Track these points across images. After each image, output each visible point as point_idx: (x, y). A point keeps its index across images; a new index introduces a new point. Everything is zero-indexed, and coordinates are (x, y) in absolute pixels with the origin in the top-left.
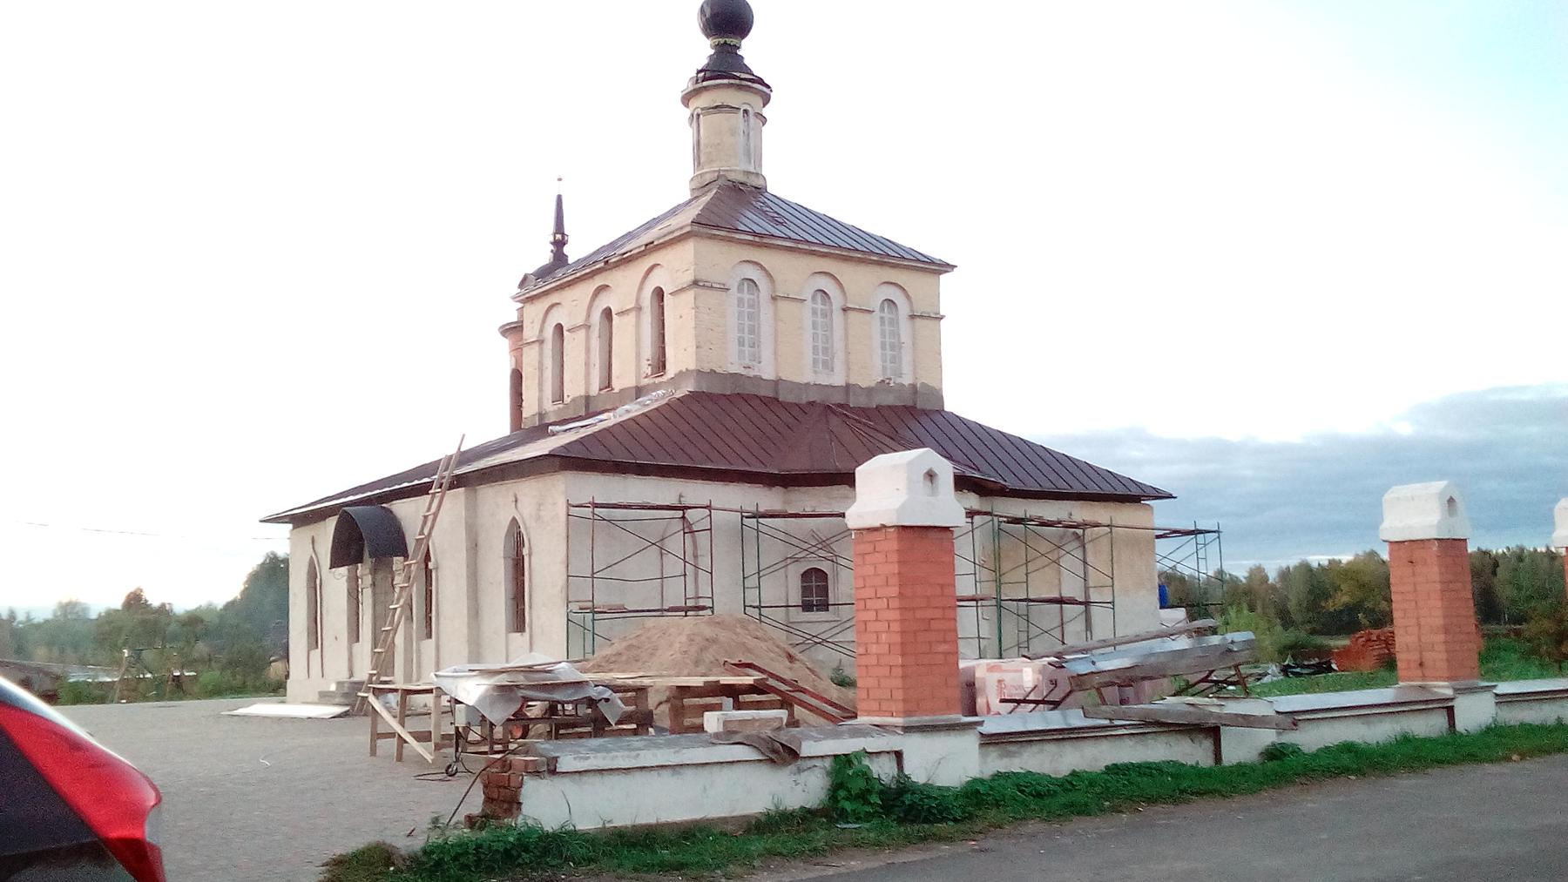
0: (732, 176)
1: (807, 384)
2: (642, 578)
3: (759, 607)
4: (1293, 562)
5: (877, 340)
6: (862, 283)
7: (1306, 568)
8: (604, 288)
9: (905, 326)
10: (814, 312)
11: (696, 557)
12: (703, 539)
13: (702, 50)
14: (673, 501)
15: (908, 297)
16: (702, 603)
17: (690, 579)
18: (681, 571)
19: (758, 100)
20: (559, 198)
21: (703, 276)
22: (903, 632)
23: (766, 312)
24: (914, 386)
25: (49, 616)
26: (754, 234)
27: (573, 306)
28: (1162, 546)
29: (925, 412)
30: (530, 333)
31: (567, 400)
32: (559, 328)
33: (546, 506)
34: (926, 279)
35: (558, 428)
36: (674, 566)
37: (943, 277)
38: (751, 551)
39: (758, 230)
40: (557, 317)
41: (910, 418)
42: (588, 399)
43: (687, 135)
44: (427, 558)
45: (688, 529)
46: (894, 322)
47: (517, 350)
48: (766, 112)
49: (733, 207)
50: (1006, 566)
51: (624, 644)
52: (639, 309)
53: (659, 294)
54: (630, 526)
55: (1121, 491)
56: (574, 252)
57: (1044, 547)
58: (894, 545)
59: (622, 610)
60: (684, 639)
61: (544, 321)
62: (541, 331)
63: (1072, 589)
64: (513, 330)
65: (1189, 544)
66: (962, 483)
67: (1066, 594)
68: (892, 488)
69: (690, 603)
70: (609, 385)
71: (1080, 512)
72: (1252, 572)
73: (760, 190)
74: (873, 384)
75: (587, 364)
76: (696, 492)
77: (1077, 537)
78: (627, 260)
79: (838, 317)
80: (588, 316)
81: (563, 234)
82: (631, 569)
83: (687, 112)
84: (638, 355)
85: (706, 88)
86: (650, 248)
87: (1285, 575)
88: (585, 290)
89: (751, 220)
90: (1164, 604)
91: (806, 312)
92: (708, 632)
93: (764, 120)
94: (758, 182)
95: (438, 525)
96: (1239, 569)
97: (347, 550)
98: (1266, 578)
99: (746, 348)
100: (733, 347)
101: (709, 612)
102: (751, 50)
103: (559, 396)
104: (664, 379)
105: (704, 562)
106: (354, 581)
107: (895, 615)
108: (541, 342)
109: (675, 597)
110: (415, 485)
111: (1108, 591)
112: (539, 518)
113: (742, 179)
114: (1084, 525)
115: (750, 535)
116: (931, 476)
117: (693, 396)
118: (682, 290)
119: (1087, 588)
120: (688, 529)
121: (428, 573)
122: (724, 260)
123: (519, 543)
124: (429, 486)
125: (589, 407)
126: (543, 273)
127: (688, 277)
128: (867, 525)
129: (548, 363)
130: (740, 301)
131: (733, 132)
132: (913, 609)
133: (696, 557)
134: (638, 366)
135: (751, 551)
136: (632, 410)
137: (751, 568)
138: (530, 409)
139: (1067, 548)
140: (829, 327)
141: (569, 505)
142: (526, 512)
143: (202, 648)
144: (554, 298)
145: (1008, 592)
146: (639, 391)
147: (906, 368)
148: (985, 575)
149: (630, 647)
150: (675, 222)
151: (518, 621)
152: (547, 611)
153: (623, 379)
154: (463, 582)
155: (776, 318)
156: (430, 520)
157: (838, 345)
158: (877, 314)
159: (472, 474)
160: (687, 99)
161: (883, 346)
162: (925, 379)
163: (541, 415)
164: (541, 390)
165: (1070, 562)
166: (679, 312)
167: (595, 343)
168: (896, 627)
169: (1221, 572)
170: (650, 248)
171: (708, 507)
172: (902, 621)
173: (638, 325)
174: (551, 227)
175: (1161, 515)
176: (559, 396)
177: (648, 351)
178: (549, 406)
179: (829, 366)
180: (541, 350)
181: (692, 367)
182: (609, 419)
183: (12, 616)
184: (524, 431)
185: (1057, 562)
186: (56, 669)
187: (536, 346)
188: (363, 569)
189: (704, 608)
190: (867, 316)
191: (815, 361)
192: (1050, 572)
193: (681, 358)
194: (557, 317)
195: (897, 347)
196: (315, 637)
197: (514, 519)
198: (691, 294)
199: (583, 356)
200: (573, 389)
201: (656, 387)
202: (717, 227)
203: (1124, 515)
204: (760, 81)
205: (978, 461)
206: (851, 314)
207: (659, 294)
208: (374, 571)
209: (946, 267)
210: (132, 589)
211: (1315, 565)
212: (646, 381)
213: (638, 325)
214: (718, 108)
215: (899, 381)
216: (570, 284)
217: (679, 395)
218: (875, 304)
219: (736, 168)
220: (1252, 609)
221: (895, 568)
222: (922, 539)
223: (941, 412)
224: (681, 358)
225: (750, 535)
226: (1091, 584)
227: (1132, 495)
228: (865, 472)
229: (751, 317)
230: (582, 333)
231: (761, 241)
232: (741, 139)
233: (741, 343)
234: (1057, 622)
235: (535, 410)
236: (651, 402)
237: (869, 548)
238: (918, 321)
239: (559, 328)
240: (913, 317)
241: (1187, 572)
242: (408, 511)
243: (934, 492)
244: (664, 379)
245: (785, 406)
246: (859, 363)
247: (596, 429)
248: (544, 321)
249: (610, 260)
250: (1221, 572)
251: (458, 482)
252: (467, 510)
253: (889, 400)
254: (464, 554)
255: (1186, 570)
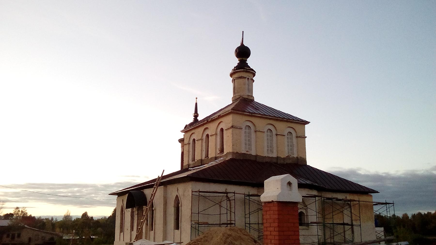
0: (244, 97)
1: (266, 157)
2: (214, 214)
3: (250, 224)
4: (416, 212)
5: (286, 143)
6: (282, 127)
7: (420, 214)
8: (207, 128)
9: (295, 140)
10: (268, 136)
11: (230, 208)
12: (233, 202)
13: (236, 61)
14: (224, 191)
15: (276, 129)
16: (232, 222)
17: (229, 214)
18: (226, 212)
19: (251, 75)
20: (196, 104)
21: (235, 125)
22: (279, 240)
23: (253, 135)
24: (297, 157)
25: (62, 219)
26: (249, 112)
27: (198, 133)
28: (376, 208)
29: (301, 166)
30: (186, 142)
31: (196, 161)
32: (194, 140)
33: (186, 192)
34: (302, 125)
35: (192, 169)
36: (224, 211)
37: (306, 126)
38: (247, 207)
39: (251, 111)
40: (194, 137)
41: (297, 167)
42: (201, 160)
43: (231, 85)
44: (153, 207)
45: (228, 199)
46: (291, 139)
47: (183, 147)
48: (254, 79)
49: (244, 105)
50: (326, 213)
51: (203, 236)
52: (216, 134)
53: (222, 130)
54: (210, 198)
55: (362, 190)
56: (200, 118)
57: (338, 207)
58: (276, 208)
59: (207, 224)
60: (221, 235)
61: (190, 138)
62: (189, 140)
63: (347, 220)
64: (181, 141)
65: (384, 207)
66: (301, 186)
67: (345, 222)
68: (275, 188)
69: (229, 222)
70: (208, 156)
71: (349, 197)
72: (403, 215)
73: (253, 100)
74: (285, 157)
75: (202, 150)
76: (231, 188)
77: (348, 204)
78: (213, 120)
79: (275, 137)
80: (202, 136)
81: (197, 114)
82: (210, 211)
83: (232, 79)
84: (216, 148)
85: (237, 72)
86: (220, 117)
87: (414, 216)
88: (201, 129)
89: (250, 109)
90: (377, 226)
91: (285, 139)
92: (229, 232)
93: (253, 81)
94: (252, 98)
95: (157, 197)
96: (399, 214)
97: (130, 205)
98: (408, 217)
99: (247, 146)
100: (243, 146)
101: (234, 225)
102: (251, 62)
103: (194, 159)
104: (223, 155)
105: (233, 210)
106: (132, 213)
107: (276, 233)
108: (189, 144)
109: (224, 220)
110: (149, 185)
111: (358, 222)
112: (184, 195)
113: (246, 97)
114: (350, 201)
115: (247, 201)
116: (289, 184)
117: (231, 160)
118: (228, 129)
119: (352, 220)
120: (228, 199)
121: (153, 211)
122: (241, 121)
123: (178, 203)
124: (154, 185)
125: (202, 162)
126: (191, 124)
127: (230, 125)
128: (267, 201)
129: (191, 150)
130: (245, 132)
131: (244, 84)
132: (283, 231)
133: (230, 208)
134: (216, 151)
135: (247, 207)
136: (213, 163)
137: (247, 212)
138: (185, 163)
139: (345, 208)
140: (272, 140)
141: (192, 192)
142: (181, 193)
143: (99, 229)
144: (193, 131)
145: (327, 221)
146: (216, 158)
147: (295, 152)
148: (320, 216)
149: (204, 237)
150: (227, 109)
151: (177, 227)
152: (186, 225)
153: (212, 155)
154: (162, 214)
155: (256, 137)
156: (153, 195)
157: (275, 145)
158: (286, 136)
159: (165, 182)
160: (231, 75)
161: (288, 146)
162: (301, 155)
163: (189, 165)
164: (189, 158)
165: (347, 212)
166: (227, 135)
167: (204, 144)
168: (277, 238)
169: (394, 215)
170: (220, 117)
171: (234, 193)
172: (279, 235)
173: (216, 139)
174: (194, 112)
175: (375, 198)
176: (194, 159)
177: (219, 147)
178: (191, 162)
179: (272, 152)
180: (189, 146)
181: (231, 151)
182: (206, 166)
183: (52, 219)
184: (183, 170)
185: (342, 212)
186: (61, 234)
187: (188, 145)
188: (135, 209)
189: (232, 224)
190: (284, 137)
191: (268, 150)
192: (340, 215)
193: (228, 149)
194: (194, 137)
195: (292, 146)
196: (122, 230)
197: (177, 196)
198: (231, 130)
199: (201, 148)
200: (198, 158)
201: (221, 157)
202: (239, 111)
203: (364, 198)
204: (252, 70)
205: (318, 181)
206: (279, 136)
207: (222, 130)
208: (138, 210)
209: (307, 123)
210: (84, 212)
211: (423, 213)
212: (218, 155)
213: (216, 139)
214: (241, 77)
215: (293, 156)
216: (197, 127)
217: (227, 159)
218: (286, 133)
219: (245, 94)
220: (404, 227)
221: (276, 216)
222: (283, 206)
223: (306, 165)
224: (228, 149)
225: (247, 201)
226: (353, 219)
227: (366, 192)
228: (267, 182)
229: (249, 137)
230: (201, 141)
231: (252, 115)
232: (247, 86)
233: (246, 144)
234: (343, 231)
235: (187, 163)
236: (218, 161)
237: (268, 209)
238: (299, 139)
239: (194, 140)
240: (297, 137)
241: (384, 215)
242: (148, 192)
243: (291, 190)
244: (223, 155)
245: (259, 163)
246: (282, 151)
247: (201, 169)
248: (190, 138)
249: (209, 120)
250: (394, 215)
251: (161, 184)
252: (164, 193)
253: (289, 162)
254: (162, 206)
255: (384, 214)
